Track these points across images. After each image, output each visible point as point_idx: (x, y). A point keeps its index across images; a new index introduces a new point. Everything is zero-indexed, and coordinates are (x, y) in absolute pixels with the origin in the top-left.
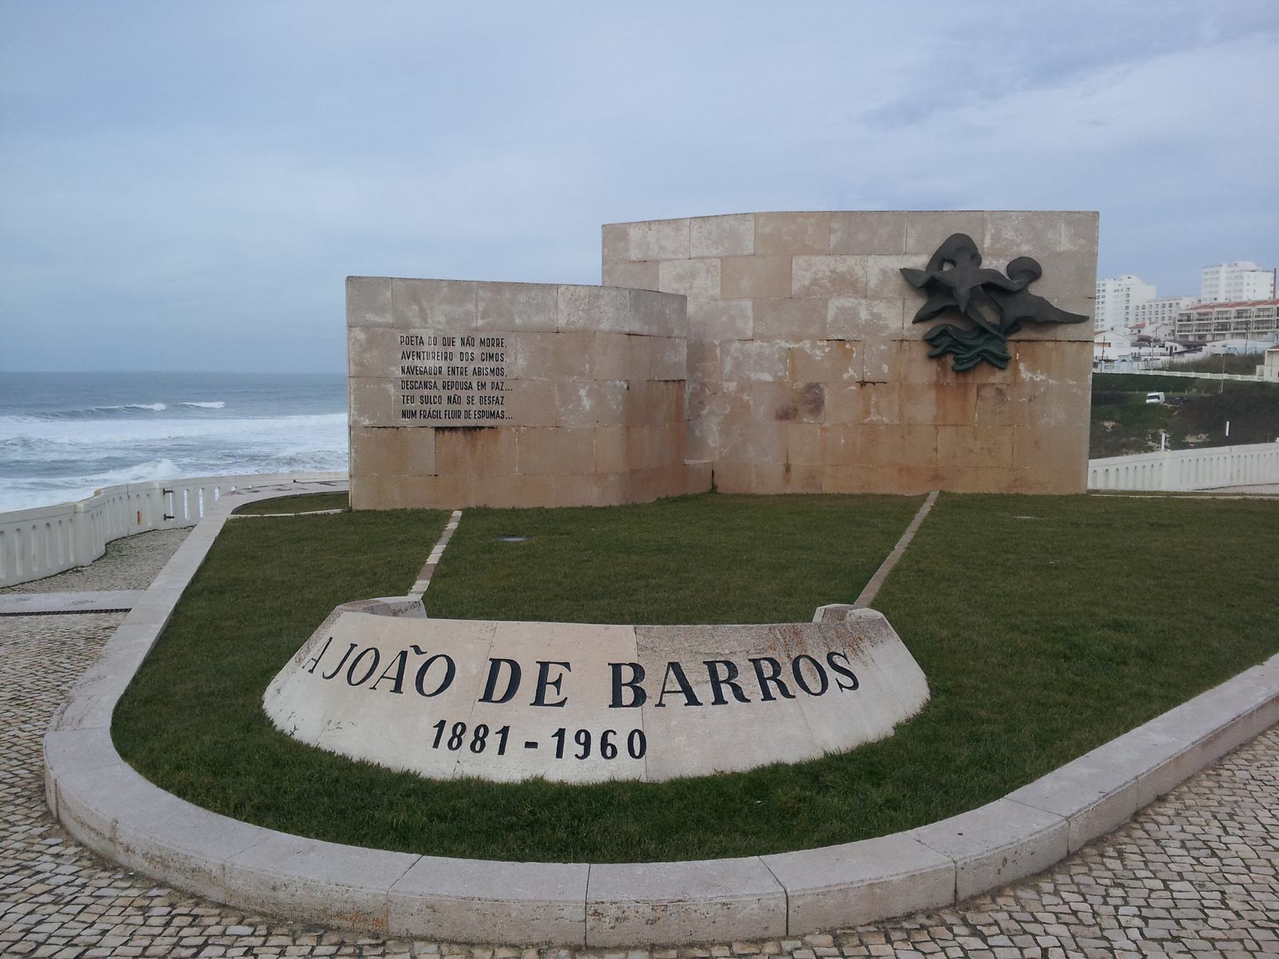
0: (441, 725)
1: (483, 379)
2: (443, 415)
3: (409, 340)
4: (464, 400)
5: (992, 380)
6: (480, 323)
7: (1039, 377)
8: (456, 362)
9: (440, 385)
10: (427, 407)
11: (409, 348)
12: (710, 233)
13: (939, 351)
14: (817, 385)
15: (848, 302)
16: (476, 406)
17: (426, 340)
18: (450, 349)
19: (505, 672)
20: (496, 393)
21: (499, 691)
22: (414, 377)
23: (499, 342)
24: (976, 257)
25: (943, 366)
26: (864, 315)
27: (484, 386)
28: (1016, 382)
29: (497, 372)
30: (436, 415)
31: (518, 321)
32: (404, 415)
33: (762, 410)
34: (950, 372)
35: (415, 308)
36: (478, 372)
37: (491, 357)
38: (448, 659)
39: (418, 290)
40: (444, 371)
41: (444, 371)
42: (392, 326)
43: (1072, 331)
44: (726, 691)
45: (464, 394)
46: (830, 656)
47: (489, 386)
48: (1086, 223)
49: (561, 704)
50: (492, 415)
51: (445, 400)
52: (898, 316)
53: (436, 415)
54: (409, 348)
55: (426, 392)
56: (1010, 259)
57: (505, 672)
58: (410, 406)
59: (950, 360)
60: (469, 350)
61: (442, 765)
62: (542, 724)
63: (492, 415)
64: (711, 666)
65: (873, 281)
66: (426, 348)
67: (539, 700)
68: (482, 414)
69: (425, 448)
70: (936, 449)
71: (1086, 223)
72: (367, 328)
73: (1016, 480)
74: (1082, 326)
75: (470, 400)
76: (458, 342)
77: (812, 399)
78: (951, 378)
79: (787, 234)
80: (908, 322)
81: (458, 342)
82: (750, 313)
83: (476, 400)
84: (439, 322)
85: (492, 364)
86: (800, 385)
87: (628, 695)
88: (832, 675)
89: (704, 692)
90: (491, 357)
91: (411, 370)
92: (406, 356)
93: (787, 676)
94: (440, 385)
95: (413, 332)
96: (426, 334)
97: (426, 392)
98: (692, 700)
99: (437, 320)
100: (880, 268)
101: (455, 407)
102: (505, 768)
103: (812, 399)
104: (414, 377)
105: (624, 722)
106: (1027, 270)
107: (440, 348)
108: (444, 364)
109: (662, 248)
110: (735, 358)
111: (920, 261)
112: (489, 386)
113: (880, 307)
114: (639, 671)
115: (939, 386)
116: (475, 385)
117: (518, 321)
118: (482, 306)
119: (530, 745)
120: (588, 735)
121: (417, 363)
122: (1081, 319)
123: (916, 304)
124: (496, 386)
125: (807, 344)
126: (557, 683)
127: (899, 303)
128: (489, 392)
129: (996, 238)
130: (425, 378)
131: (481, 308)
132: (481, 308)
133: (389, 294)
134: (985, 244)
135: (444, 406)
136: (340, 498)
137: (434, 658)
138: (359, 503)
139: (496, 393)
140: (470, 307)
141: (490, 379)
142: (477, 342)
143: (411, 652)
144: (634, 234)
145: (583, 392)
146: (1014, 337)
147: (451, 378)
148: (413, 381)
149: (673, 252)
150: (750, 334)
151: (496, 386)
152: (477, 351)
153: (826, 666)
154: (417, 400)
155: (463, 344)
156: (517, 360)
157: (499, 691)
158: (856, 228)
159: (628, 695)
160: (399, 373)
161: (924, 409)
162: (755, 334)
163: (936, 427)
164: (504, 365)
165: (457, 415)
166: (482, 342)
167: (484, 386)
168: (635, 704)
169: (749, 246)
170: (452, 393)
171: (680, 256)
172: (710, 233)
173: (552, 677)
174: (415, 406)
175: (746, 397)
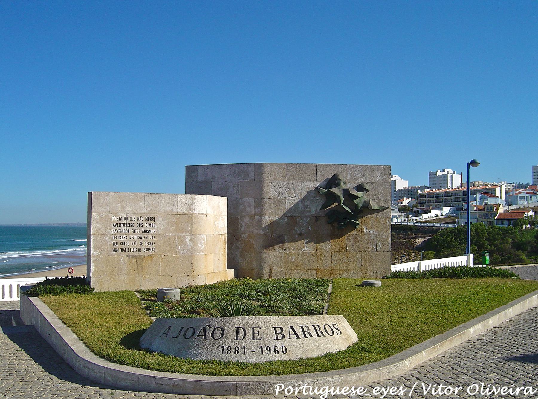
0: (223, 347)
2: (129, 250)
3: (116, 218)
4: (138, 244)
6: (145, 211)
7: (370, 232)
8: (136, 228)
9: (128, 237)
11: (116, 222)
12: (235, 171)
14: (282, 235)
16: (143, 246)
17: (123, 218)
18: (133, 222)
19: (241, 331)
22: (118, 234)
23: (153, 219)
28: (362, 234)
31: (161, 210)
36: (144, 231)
37: (150, 225)
38: (221, 329)
44: (307, 335)
45: (138, 241)
46: (333, 325)
57: (241, 331)
58: (116, 247)
59: (336, 224)
60: (141, 222)
64: (302, 327)
68: (146, 249)
75: (141, 244)
81: (136, 219)
83: (143, 244)
85: (151, 228)
87: (280, 336)
88: (334, 330)
89: (301, 334)
90: (150, 225)
91: (116, 231)
92: (115, 225)
93: (322, 330)
94: (128, 237)
95: (118, 215)
96: (124, 215)
98: (298, 337)
101: (135, 247)
104: (118, 234)
107: (129, 221)
112: (149, 238)
114: (282, 329)
116: (143, 237)
118: (146, 203)
120: (270, 348)
124: (152, 237)
128: (149, 240)
130: (121, 235)
135: (130, 246)
142: (144, 219)
144: (200, 171)
147: (134, 234)
151: (152, 237)
152: (144, 222)
153: (332, 327)
154: (119, 244)
156: (160, 226)
159: (280, 336)
160: (112, 232)
162: (256, 213)
168: (282, 339)
172: (235, 171)
175: (251, 241)
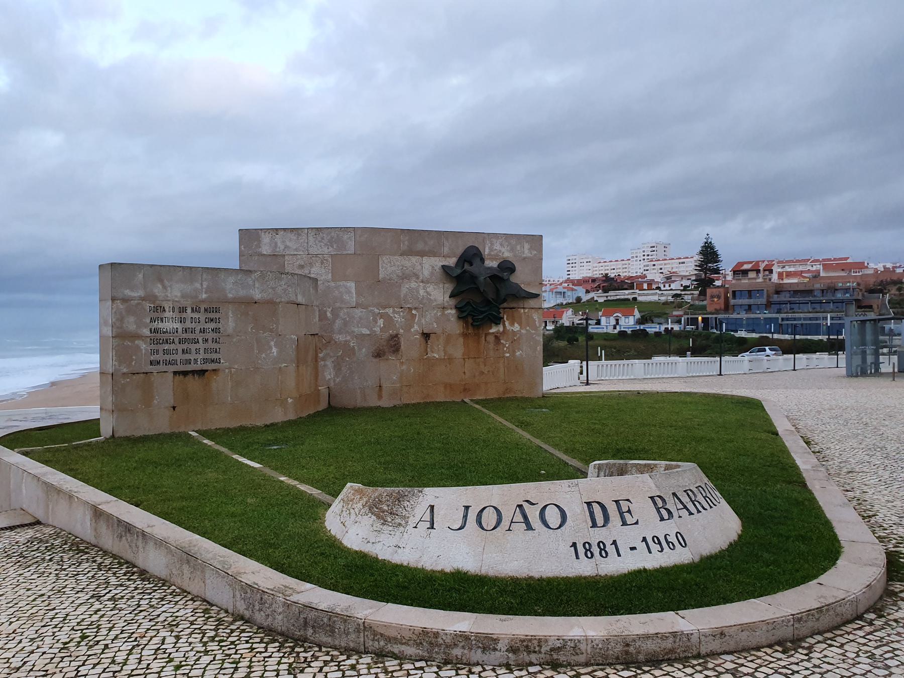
1: (206, 336)
5: (491, 331)
6: (204, 296)
8: (188, 324)
9: (177, 340)
10: (167, 357)
11: (155, 315)
13: (465, 314)
15: (413, 285)
18: (184, 315)
21: (600, 520)
22: (158, 336)
24: (482, 260)
25: (466, 323)
26: (422, 292)
27: (207, 340)
30: (174, 363)
32: (151, 364)
33: (363, 352)
35: (160, 286)
36: (203, 331)
39: (160, 272)
40: (180, 330)
41: (180, 330)
42: (143, 299)
43: (532, 303)
45: (193, 347)
47: (210, 341)
48: (536, 241)
49: (637, 523)
51: (180, 351)
52: (441, 294)
53: (174, 363)
54: (155, 315)
55: (166, 347)
56: (499, 261)
59: (470, 320)
61: (585, 568)
62: (627, 536)
65: (426, 273)
66: (168, 314)
67: (624, 523)
68: (205, 361)
69: (165, 389)
72: (125, 300)
74: (535, 300)
75: (197, 351)
76: (189, 310)
77: (393, 345)
80: (447, 298)
81: (189, 310)
82: (353, 291)
83: (202, 351)
85: (212, 325)
86: (386, 335)
90: (212, 320)
91: (156, 331)
94: (177, 340)
97: (166, 347)
100: (431, 265)
101: (187, 356)
102: (614, 566)
103: (393, 345)
105: (669, 528)
106: (508, 267)
107: (176, 315)
109: (286, 247)
110: (344, 319)
112: (210, 341)
113: (430, 288)
115: (465, 335)
116: (200, 341)
117: (230, 296)
118: (205, 285)
119: (633, 549)
121: (161, 325)
122: (536, 296)
123: (449, 287)
124: (215, 341)
125: (390, 311)
126: (629, 511)
128: (210, 345)
129: (491, 249)
133: (141, 276)
135: (179, 357)
136: (91, 426)
137: (484, 508)
141: (210, 336)
142: (202, 310)
143: (525, 505)
145: (272, 343)
147: (185, 336)
149: (296, 250)
150: (354, 305)
152: (202, 316)
154: (161, 352)
157: (600, 520)
158: (414, 242)
159: (665, 514)
160: (148, 333)
161: (458, 350)
164: (220, 325)
165: (188, 362)
166: (206, 310)
167: (207, 340)
169: (351, 248)
170: (185, 346)
173: (625, 509)
174: (160, 357)
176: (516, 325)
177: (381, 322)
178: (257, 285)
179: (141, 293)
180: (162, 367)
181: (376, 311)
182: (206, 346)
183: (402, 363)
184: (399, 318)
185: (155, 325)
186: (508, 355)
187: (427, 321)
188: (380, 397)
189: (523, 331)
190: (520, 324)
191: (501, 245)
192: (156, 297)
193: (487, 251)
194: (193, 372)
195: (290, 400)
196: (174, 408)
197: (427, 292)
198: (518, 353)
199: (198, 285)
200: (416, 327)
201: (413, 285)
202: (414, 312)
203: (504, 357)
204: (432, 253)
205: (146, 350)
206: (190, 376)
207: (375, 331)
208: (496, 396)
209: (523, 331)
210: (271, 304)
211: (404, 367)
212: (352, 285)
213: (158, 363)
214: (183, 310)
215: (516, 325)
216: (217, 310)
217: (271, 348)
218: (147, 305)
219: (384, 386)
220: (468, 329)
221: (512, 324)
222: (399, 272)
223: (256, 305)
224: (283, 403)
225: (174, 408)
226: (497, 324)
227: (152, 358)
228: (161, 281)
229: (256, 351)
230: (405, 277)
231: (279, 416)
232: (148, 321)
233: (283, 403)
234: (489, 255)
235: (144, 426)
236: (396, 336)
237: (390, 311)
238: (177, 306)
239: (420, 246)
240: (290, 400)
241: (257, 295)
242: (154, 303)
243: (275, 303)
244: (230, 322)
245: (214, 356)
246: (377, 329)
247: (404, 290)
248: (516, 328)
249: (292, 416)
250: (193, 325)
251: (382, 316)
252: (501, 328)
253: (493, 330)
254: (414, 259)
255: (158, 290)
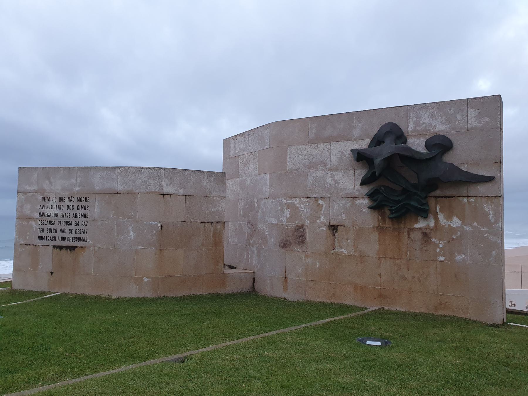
5: (417, 226)
6: (78, 189)
8: (65, 211)
9: (56, 223)
10: (49, 235)
11: (43, 203)
16: (73, 235)
18: (62, 204)
20: (84, 228)
22: (44, 218)
25: (383, 216)
26: (329, 181)
29: (85, 216)
32: (39, 239)
33: (273, 241)
34: (387, 220)
35: (47, 182)
36: (75, 216)
37: (82, 207)
40: (59, 215)
41: (59, 215)
42: (36, 192)
43: (482, 189)
45: (68, 228)
48: (492, 105)
50: (81, 240)
51: (58, 231)
54: (43, 203)
55: (49, 227)
56: (428, 137)
63: (81, 240)
65: (334, 160)
66: (51, 203)
68: (76, 239)
69: (47, 257)
70: (380, 275)
71: (492, 105)
72: (25, 193)
73: (441, 304)
74: (489, 185)
75: (71, 231)
76: (66, 200)
78: (388, 224)
79: (282, 136)
80: (358, 187)
81: (66, 200)
83: (74, 232)
84: (58, 190)
85: (82, 212)
86: (292, 226)
90: (82, 207)
91: (43, 215)
94: (56, 223)
99: (57, 186)
100: (341, 151)
101: (63, 235)
103: (297, 237)
104: (44, 218)
106: (441, 145)
108: (59, 211)
111: (363, 144)
112: (80, 224)
113: (339, 176)
115: (380, 230)
116: (73, 223)
118: (79, 180)
121: (47, 211)
122: (489, 179)
123: (361, 173)
124: (84, 224)
125: (296, 201)
127: (351, 172)
128: (80, 227)
129: (417, 124)
130: (50, 219)
131: (78, 181)
132: (78, 181)
134: (409, 127)
135: (58, 235)
138: (16, 286)
139: (84, 228)
140: (73, 181)
141: (80, 220)
142: (76, 199)
146: (433, 194)
147: (63, 219)
148: (45, 220)
152: (75, 204)
154: (45, 231)
155: (69, 200)
158: (322, 129)
161: (371, 246)
163: (379, 258)
165: (63, 239)
166: (78, 200)
167: (78, 223)
171: (246, 153)
174: (44, 234)
176: (455, 219)
177: (287, 212)
178: (119, 179)
179: (35, 188)
180: (45, 242)
181: (284, 201)
182: (77, 227)
183: (307, 256)
184: (304, 208)
185: (43, 210)
186: (442, 258)
187: (334, 211)
188: (286, 289)
189: (467, 228)
190: (462, 218)
191: (432, 116)
192: (45, 190)
193: (411, 127)
194: (67, 247)
195: (146, 279)
196: (52, 273)
197: (336, 182)
198: (458, 258)
199: (73, 181)
200: (322, 218)
201: (320, 173)
202: (320, 202)
203: (435, 260)
204: (342, 138)
205: (36, 228)
206: (64, 250)
207: (282, 221)
208: (423, 310)
209: (467, 228)
210: (131, 194)
211: (309, 261)
212: (267, 177)
213: (43, 238)
214: (62, 199)
215: (455, 219)
216: (86, 200)
217: (128, 232)
218: (39, 196)
219: (289, 277)
220: (384, 221)
221: (449, 218)
222: (306, 162)
223: (118, 195)
224: (138, 280)
225: (52, 273)
226: (426, 217)
227: (39, 235)
228: (49, 179)
229: (116, 234)
230: (312, 166)
231: (132, 291)
232: (39, 207)
233: (138, 280)
234: (414, 131)
235: (31, 284)
236: (302, 226)
237: (296, 201)
238: (58, 196)
239: (329, 132)
240: (146, 279)
241: (119, 188)
242: (43, 194)
243: (135, 193)
244: (96, 209)
245: (82, 236)
246: (284, 220)
247: (310, 180)
248: (456, 222)
249: (149, 295)
250: (69, 211)
251: (288, 206)
252: (432, 223)
253: (421, 224)
254: (322, 146)
255: (46, 185)
